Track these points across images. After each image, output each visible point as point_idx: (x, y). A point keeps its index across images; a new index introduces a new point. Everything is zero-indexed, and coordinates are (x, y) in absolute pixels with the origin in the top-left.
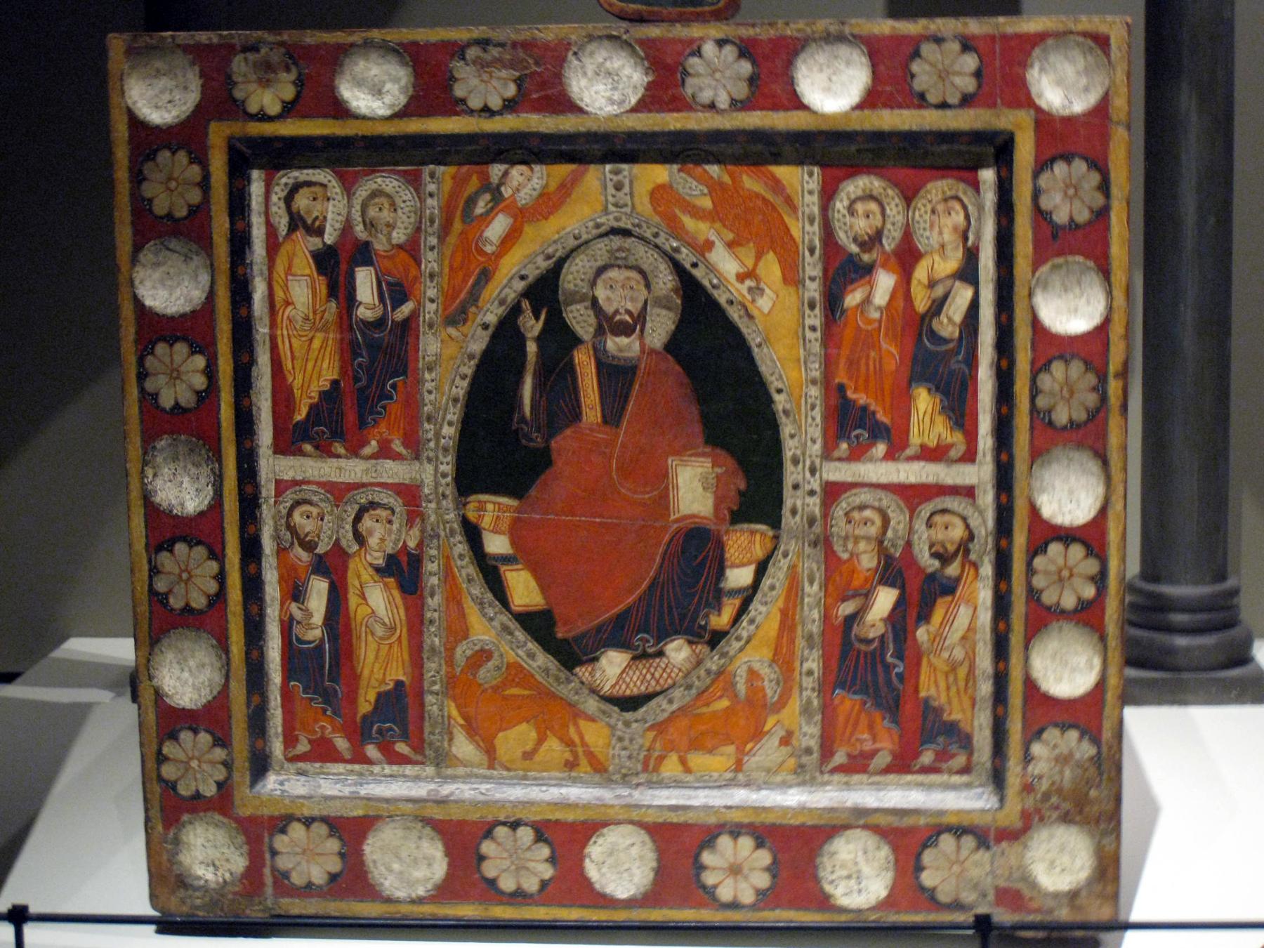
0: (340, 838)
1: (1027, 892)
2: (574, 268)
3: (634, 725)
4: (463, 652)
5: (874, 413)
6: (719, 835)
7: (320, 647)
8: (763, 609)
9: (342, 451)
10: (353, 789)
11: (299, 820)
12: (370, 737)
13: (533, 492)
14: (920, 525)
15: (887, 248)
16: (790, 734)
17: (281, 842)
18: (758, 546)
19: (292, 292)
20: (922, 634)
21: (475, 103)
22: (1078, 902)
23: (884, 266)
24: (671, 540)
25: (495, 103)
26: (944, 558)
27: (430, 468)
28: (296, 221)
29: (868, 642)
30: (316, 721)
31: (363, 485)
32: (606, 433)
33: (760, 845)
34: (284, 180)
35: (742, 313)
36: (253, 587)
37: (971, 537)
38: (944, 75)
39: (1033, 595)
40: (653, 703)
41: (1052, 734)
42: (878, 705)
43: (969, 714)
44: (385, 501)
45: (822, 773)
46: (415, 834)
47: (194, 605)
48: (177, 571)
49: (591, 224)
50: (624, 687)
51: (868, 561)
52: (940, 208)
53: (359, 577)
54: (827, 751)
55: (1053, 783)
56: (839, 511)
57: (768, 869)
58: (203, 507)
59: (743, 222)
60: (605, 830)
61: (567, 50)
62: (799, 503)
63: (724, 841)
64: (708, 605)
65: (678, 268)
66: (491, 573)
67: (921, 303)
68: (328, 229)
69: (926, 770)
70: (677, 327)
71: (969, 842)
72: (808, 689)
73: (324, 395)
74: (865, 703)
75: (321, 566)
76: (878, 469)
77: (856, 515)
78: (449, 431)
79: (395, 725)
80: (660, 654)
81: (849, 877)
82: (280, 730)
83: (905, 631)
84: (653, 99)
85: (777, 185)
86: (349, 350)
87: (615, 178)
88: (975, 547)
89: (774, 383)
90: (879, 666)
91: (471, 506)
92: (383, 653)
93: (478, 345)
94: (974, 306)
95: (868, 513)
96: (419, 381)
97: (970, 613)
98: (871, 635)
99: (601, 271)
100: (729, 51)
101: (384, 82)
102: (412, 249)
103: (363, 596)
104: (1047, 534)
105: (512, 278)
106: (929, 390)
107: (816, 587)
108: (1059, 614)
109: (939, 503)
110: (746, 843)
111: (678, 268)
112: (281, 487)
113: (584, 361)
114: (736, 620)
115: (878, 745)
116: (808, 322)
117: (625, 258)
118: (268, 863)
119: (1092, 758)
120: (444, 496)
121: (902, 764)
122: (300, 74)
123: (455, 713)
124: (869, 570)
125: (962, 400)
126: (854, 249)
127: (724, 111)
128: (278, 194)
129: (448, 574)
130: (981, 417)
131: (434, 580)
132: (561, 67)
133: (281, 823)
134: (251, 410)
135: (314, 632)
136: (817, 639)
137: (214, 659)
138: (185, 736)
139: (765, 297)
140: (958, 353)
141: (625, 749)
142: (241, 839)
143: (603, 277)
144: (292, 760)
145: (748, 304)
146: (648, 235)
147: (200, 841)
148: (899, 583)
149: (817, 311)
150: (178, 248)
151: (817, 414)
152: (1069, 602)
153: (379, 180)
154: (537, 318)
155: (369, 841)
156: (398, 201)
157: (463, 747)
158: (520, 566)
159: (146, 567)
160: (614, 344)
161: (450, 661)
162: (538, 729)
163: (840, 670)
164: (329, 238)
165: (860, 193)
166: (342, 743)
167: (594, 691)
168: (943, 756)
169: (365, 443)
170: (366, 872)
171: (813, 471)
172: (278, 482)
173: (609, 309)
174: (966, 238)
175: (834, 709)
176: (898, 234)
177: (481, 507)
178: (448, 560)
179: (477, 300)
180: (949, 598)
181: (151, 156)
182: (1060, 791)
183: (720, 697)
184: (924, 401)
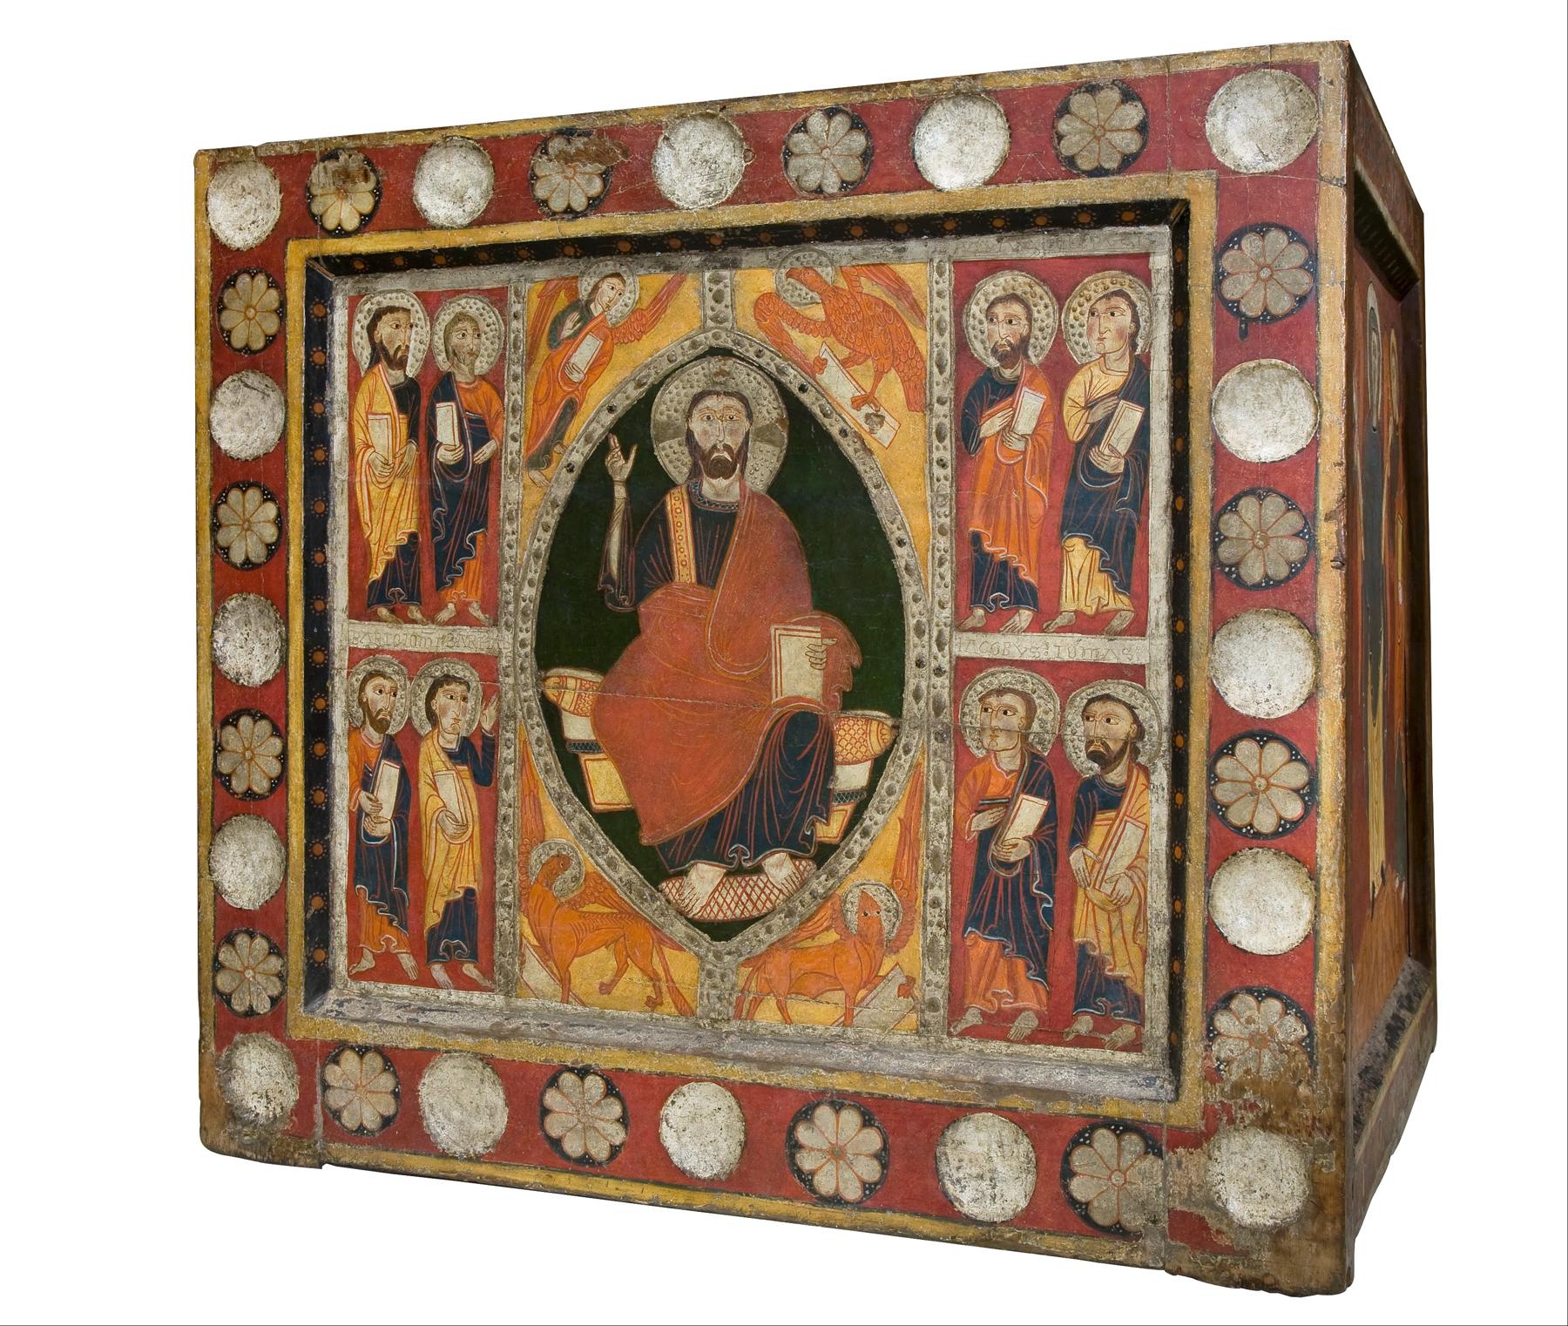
0: (395, 1073)
1: (1211, 1222)
2: (667, 397)
3: (727, 958)
4: (538, 857)
5: (1016, 570)
6: (818, 1105)
7: (389, 844)
8: (879, 818)
9: (418, 616)
10: (414, 1015)
11: (352, 1048)
12: (436, 955)
13: (619, 666)
14: (1074, 716)
15: (1034, 360)
16: (911, 980)
17: (333, 1074)
18: (874, 739)
19: (370, 431)
20: (1077, 859)
21: (558, 204)
22: (1284, 1243)
23: (1030, 383)
24: (773, 728)
25: (579, 203)
26: (1104, 759)
27: (508, 636)
28: (379, 353)
29: (1009, 866)
30: (381, 932)
31: (439, 655)
32: (700, 595)
33: (867, 1123)
34: (367, 306)
35: (858, 446)
36: (318, 772)
37: (1141, 733)
38: (1099, 133)
39: (1217, 810)
40: (750, 929)
41: (1244, 1003)
42: (1021, 951)
43: (1138, 969)
44: (461, 674)
45: (950, 1035)
46: (476, 1076)
47: (255, 789)
48: (240, 750)
49: (687, 343)
50: (716, 909)
51: (1010, 762)
52: (1101, 307)
53: (431, 763)
54: (956, 1008)
55: (1247, 1072)
56: (972, 697)
57: (876, 1156)
58: (269, 677)
59: (860, 335)
60: (685, 1088)
61: (658, 135)
62: (924, 685)
63: (824, 1113)
64: (815, 811)
65: (784, 392)
66: (570, 759)
67: (1076, 427)
68: (410, 360)
69: (1081, 1042)
70: (783, 465)
71: (1133, 1142)
72: (932, 927)
73: (402, 550)
74: (1005, 947)
75: (391, 750)
76: (1020, 642)
77: (993, 700)
78: (530, 592)
79: (462, 937)
80: (758, 870)
81: (981, 1177)
82: (344, 941)
83: (1055, 856)
84: (753, 187)
85: (900, 288)
86: (429, 498)
87: (715, 288)
88: (1146, 747)
89: (893, 532)
90: (1022, 899)
91: (551, 682)
92: (454, 854)
93: (562, 492)
94: (1144, 430)
95: (1008, 699)
96: (499, 534)
97: (1137, 834)
98: (1013, 859)
99: (697, 399)
100: (840, 121)
101: (467, 188)
102: (494, 379)
103: (435, 787)
104: (1237, 730)
105: (598, 412)
106: (1086, 544)
107: (944, 792)
108: (1253, 837)
109: (1099, 689)
110: (851, 1118)
111: (784, 392)
112: (356, 655)
113: (677, 508)
114: (848, 831)
115: (1020, 1004)
116: (936, 455)
117: (724, 383)
118: (319, 1098)
119: (1299, 1042)
120: (523, 669)
121: (1051, 1031)
122: (378, 182)
123: (527, 931)
124: (1008, 773)
125: (1128, 554)
126: (993, 362)
127: (832, 196)
128: (362, 320)
129: (524, 762)
130: (1152, 576)
131: (510, 770)
132: (651, 154)
133: (334, 1052)
134: (325, 568)
135: (383, 827)
136: (944, 860)
137: (276, 853)
138: (242, 940)
139: (885, 427)
140: (1122, 494)
141: (714, 987)
142: (293, 1067)
143: (700, 406)
144: (357, 977)
145: (864, 435)
146: (751, 355)
147: (255, 1067)
148: (1047, 791)
149: (947, 442)
150: (256, 384)
151: (946, 570)
152: (1266, 823)
153: (463, 302)
154: (626, 458)
155: (426, 1080)
156: (482, 326)
157: (536, 974)
158: (601, 756)
159: (211, 744)
160: (715, 488)
161: (525, 868)
162: (616, 954)
163: (973, 902)
164: (412, 370)
165: (1000, 293)
166: (407, 961)
167: (681, 913)
168: (1105, 1024)
169: (441, 606)
170: (422, 1118)
171: (940, 646)
172: (352, 650)
173: (706, 445)
174: (1134, 346)
175: (966, 953)
176: (1048, 344)
177: (562, 687)
178: (524, 749)
179: (562, 438)
180: (1112, 814)
181: (231, 283)
182: (1256, 1083)
183: (827, 929)
184: (1079, 555)
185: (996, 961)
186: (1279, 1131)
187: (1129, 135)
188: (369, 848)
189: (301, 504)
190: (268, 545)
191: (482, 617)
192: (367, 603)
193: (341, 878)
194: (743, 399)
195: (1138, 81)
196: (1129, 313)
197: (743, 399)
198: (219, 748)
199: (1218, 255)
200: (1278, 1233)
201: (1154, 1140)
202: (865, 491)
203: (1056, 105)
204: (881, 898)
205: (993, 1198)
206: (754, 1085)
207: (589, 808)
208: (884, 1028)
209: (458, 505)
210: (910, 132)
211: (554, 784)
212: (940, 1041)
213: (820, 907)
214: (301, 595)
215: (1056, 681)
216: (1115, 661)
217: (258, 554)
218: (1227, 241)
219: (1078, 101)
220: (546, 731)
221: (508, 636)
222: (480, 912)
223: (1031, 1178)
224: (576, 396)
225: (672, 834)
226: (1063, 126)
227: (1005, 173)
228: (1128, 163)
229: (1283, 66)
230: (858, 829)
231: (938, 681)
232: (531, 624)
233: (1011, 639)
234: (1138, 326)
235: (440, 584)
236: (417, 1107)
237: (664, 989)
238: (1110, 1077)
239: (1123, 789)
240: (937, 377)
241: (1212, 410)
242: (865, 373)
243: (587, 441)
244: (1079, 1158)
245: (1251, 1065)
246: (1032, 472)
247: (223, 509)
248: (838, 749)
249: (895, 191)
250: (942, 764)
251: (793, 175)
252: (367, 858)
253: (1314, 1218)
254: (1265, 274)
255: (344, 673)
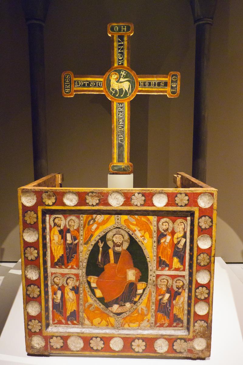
0: (63, 340)
1: (193, 350)
2: (109, 234)
4: (87, 304)
5: (166, 262)
6: (135, 339)
8: (144, 297)
9: (64, 267)
13: (100, 276)
14: (174, 282)
15: (169, 231)
16: (149, 320)
19: (54, 239)
20: (174, 302)
21: (91, 204)
22: (203, 352)
23: (169, 235)
25: (94, 204)
26: (179, 288)
27: (81, 271)
28: (55, 224)
29: (164, 303)
34: (53, 217)
36: (46, 293)
37: (184, 285)
38: (181, 200)
40: (123, 314)
42: (166, 315)
43: (183, 317)
48: (31, 290)
51: (164, 289)
52: (180, 224)
53: (67, 291)
54: (156, 323)
55: (199, 331)
56: (159, 280)
57: (145, 346)
58: (37, 278)
62: (151, 278)
66: (92, 290)
67: (175, 242)
69: (174, 327)
71: (183, 341)
72: (152, 312)
73: (60, 257)
75: (60, 289)
76: (166, 272)
79: (74, 318)
80: (125, 305)
81: (160, 347)
82: (52, 318)
85: (148, 220)
86: (65, 249)
87: (117, 218)
88: (185, 286)
89: (147, 256)
91: (89, 278)
94: (186, 242)
95: (164, 280)
96: (79, 255)
98: (165, 302)
99: (114, 235)
100: (140, 195)
102: (78, 230)
104: (199, 285)
106: (177, 258)
107: (154, 293)
112: (52, 274)
113: (111, 252)
114: (139, 299)
116: (154, 245)
117: (119, 233)
119: (206, 326)
120: (84, 276)
121: (170, 325)
123: (85, 315)
126: (163, 232)
129: (84, 290)
133: (52, 337)
141: (117, 322)
142: (44, 340)
143: (115, 236)
145: (142, 242)
146: (124, 228)
151: (155, 262)
153: (71, 217)
154: (102, 244)
156: (75, 221)
159: (25, 289)
160: (117, 249)
161: (85, 306)
162: (101, 318)
164: (62, 228)
165: (164, 221)
166: (63, 321)
168: (178, 324)
169: (68, 266)
171: (154, 273)
172: (51, 273)
174: (184, 230)
176: (171, 229)
177: (91, 278)
179: (90, 240)
182: (200, 332)
183: (136, 313)
184: (176, 260)
185: (162, 317)
186: (203, 338)
187: (186, 201)
188: (56, 304)
189: (42, 251)
190: (36, 257)
191: (76, 268)
192: (54, 265)
193: (51, 309)
194: (122, 235)
195: (188, 193)
196: (184, 225)
197: (122, 235)
198: (27, 290)
199: (199, 219)
200: (202, 351)
201: (185, 340)
202: (142, 250)
203: (175, 195)
204: (144, 309)
205: (162, 349)
206: (125, 337)
207: (96, 297)
208: (145, 327)
209: (71, 251)
210: (152, 198)
211: (90, 293)
212: (153, 328)
213: (135, 310)
214: (43, 266)
215: (172, 278)
216: (180, 275)
217: (34, 258)
218: (200, 217)
219: (178, 195)
220: (88, 285)
221: (81, 271)
222: (77, 313)
223: (168, 347)
224: (93, 234)
225: (110, 301)
226: (176, 199)
227: (167, 205)
228: (186, 205)
229: (209, 193)
230: (141, 299)
231: (153, 278)
232: (85, 269)
233: (165, 272)
234: (185, 227)
235: (68, 262)
236: (67, 344)
237: (109, 323)
238: (181, 332)
239: (181, 292)
240: (154, 233)
241: (197, 241)
242: (143, 232)
243: (95, 241)
244: (175, 344)
245: (200, 330)
246: (169, 248)
247: (26, 251)
248: (138, 288)
249: (149, 206)
250: (154, 290)
251: (132, 202)
252: (55, 306)
253: (207, 348)
254: (205, 222)
255: (50, 276)
